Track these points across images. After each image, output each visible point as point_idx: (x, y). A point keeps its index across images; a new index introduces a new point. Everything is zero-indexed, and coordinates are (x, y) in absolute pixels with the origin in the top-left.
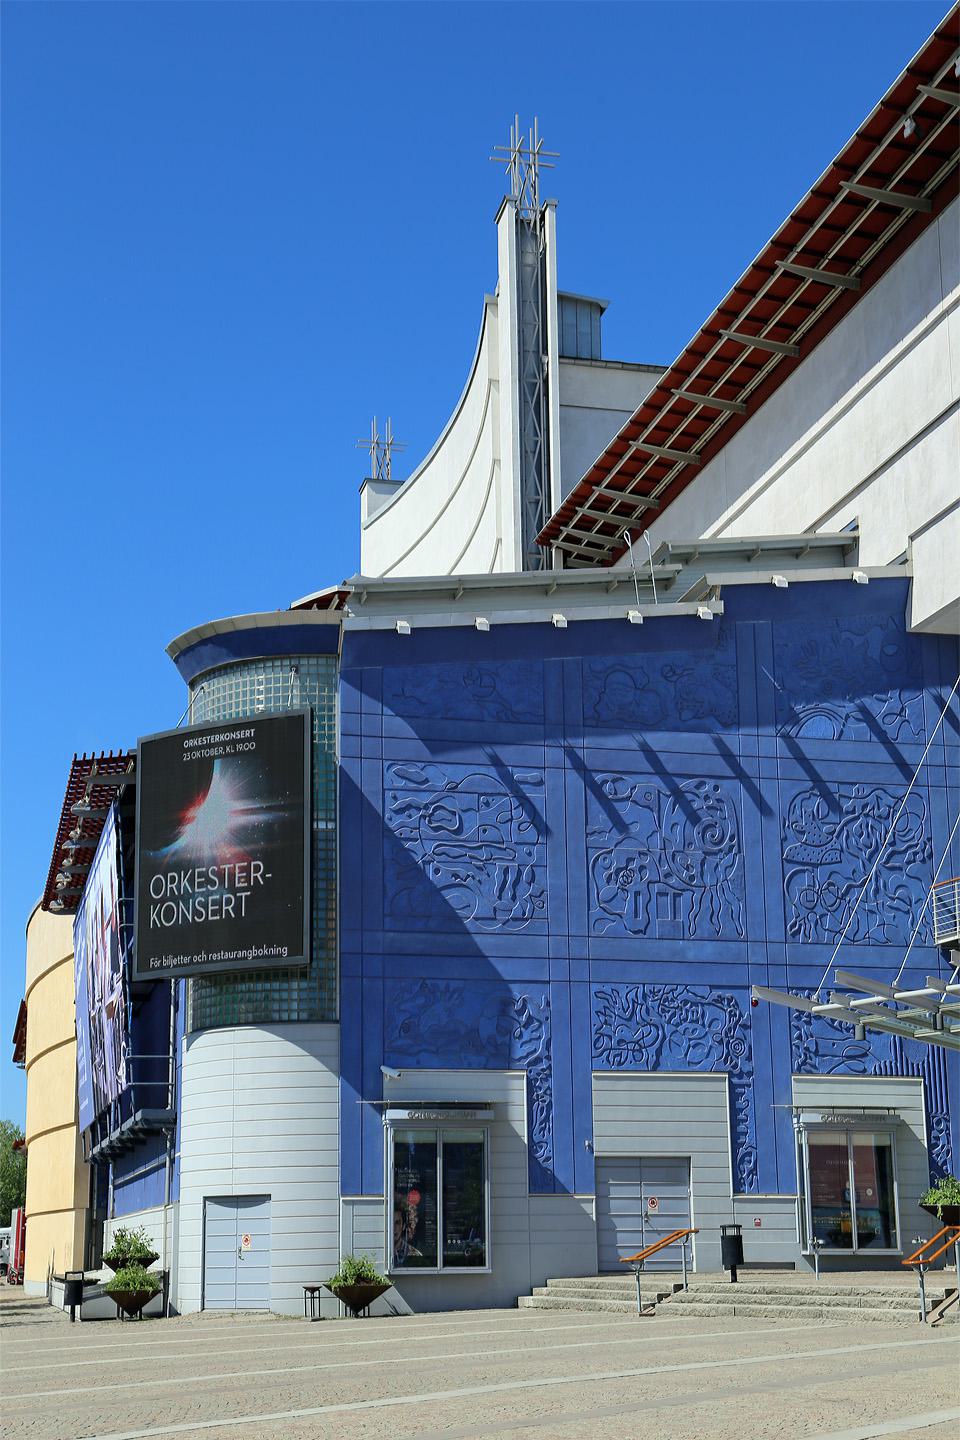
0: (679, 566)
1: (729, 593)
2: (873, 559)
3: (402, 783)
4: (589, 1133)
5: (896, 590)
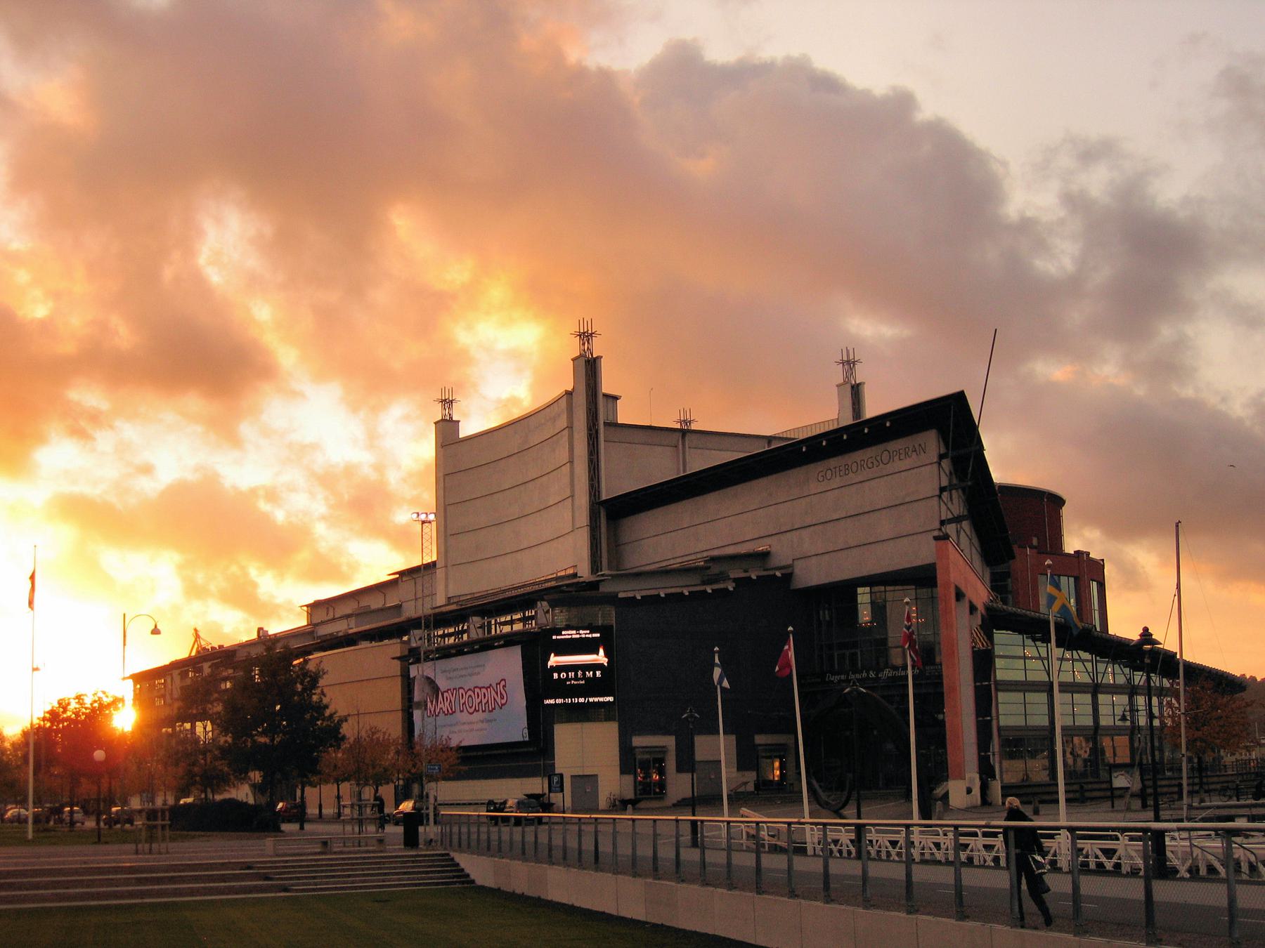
1: (735, 580)
4: (693, 754)
5: (788, 577)
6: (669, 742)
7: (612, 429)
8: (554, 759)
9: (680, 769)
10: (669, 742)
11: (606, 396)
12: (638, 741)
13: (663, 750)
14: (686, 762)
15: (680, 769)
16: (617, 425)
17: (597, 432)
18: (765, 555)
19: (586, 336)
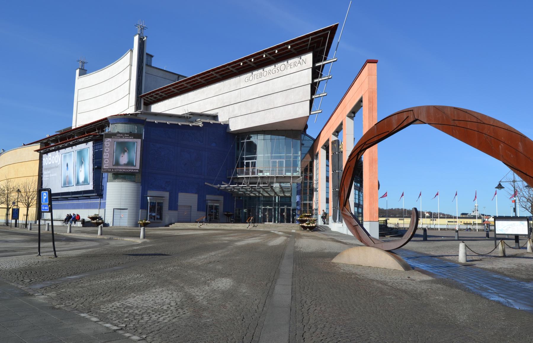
2: (222, 120)
4: (177, 202)
5: (226, 126)
6: (166, 195)
7: (149, 68)
8: (105, 199)
9: (170, 208)
10: (166, 195)
11: (147, 54)
12: (150, 193)
14: (173, 206)
15: (170, 208)
17: (142, 68)
18: (215, 117)
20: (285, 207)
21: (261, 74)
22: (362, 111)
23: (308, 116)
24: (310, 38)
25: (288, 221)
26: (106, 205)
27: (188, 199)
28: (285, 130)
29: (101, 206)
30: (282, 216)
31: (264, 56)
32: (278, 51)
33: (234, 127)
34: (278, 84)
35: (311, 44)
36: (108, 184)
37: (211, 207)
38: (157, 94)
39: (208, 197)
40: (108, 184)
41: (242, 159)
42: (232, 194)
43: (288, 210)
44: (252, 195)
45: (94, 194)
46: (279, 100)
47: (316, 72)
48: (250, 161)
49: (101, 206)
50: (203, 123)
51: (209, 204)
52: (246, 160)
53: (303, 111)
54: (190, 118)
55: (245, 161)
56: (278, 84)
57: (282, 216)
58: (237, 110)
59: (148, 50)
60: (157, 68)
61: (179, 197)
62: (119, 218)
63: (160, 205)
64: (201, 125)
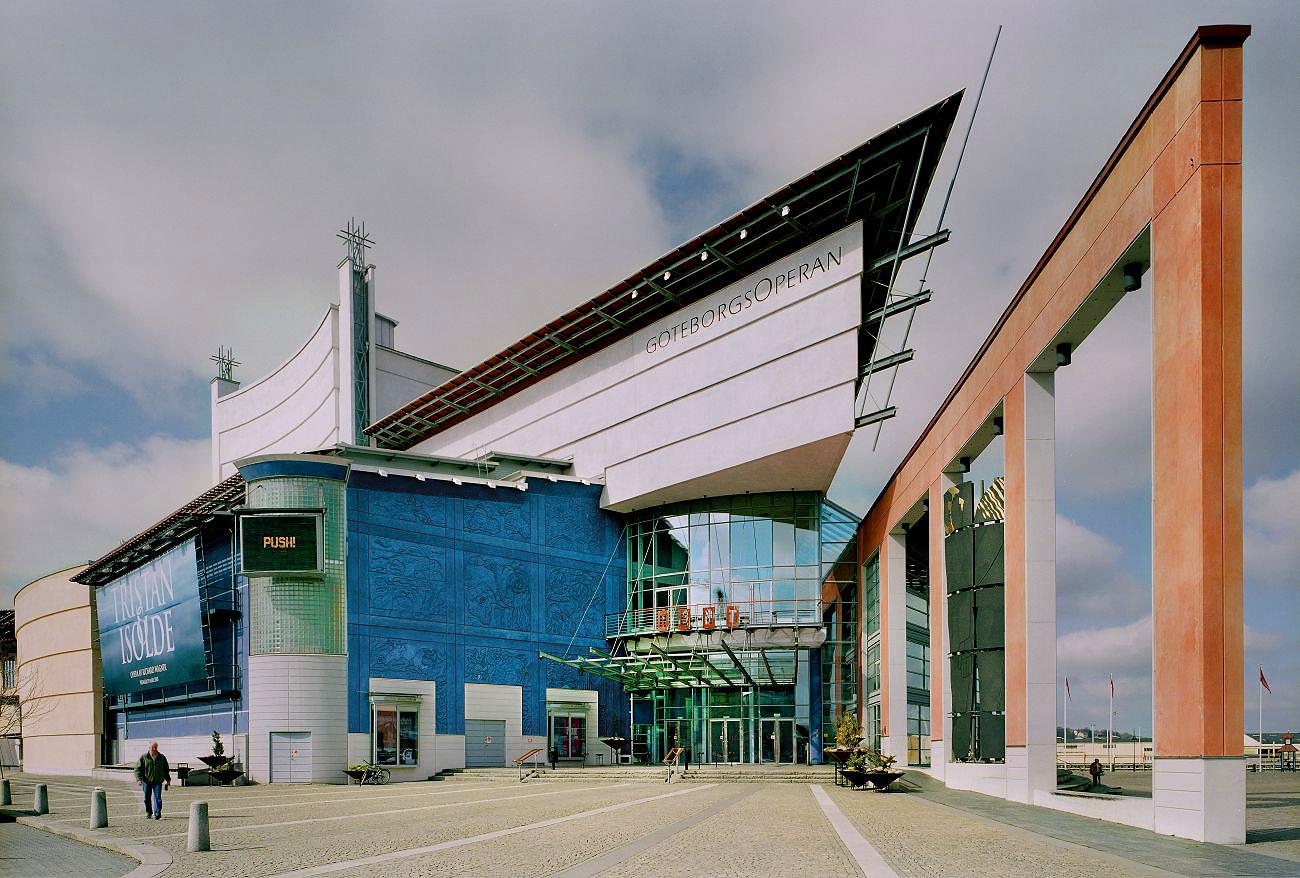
0: (497, 464)
1: (529, 480)
2: (583, 475)
3: (378, 546)
5: (597, 491)
6: (428, 689)
7: (386, 355)
9: (441, 728)
10: (428, 689)
12: (376, 684)
13: (413, 698)
14: (451, 719)
15: (441, 728)
16: (392, 351)
18: (565, 468)
19: (357, 241)
20: (777, 718)
21: (695, 321)
22: (965, 448)
23: (850, 434)
24: (856, 167)
25: (786, 758)
26: (21, 638)
27: (495, 702)
28: (772, 494)
29: (238, 725)
30: (768, 744)
31: (704, 257)
32: (751, 233)
33: (617, 495)
34: (758, 343)
35: (859, 193)
36: (251, 660)
37: (561, 722)
38: (408, 422)
39: (552, 694)
40: (251, 660)
41: (648, 584)
42: (1236, 314)
43: (786, 728)
44: (679, 685)
45: (212, 693)
46: (753, 392)
47: (874, 291)
48: (670, 589)
49: (238, 725)
50: (529, 480)
51: (554, 714)
52: (660, 586)
53: (831, 416)
54: (491, 469)
55: (656, 590)
56: (758, 343)
57: (768, 744)
58: (628, 440)
59: (379, 305)
60: (407, 356)
61: (250, 667)
62: (288, 760)
63: (411, 718)
64: (523, 486)
